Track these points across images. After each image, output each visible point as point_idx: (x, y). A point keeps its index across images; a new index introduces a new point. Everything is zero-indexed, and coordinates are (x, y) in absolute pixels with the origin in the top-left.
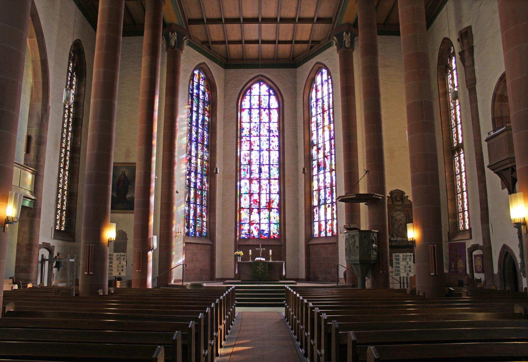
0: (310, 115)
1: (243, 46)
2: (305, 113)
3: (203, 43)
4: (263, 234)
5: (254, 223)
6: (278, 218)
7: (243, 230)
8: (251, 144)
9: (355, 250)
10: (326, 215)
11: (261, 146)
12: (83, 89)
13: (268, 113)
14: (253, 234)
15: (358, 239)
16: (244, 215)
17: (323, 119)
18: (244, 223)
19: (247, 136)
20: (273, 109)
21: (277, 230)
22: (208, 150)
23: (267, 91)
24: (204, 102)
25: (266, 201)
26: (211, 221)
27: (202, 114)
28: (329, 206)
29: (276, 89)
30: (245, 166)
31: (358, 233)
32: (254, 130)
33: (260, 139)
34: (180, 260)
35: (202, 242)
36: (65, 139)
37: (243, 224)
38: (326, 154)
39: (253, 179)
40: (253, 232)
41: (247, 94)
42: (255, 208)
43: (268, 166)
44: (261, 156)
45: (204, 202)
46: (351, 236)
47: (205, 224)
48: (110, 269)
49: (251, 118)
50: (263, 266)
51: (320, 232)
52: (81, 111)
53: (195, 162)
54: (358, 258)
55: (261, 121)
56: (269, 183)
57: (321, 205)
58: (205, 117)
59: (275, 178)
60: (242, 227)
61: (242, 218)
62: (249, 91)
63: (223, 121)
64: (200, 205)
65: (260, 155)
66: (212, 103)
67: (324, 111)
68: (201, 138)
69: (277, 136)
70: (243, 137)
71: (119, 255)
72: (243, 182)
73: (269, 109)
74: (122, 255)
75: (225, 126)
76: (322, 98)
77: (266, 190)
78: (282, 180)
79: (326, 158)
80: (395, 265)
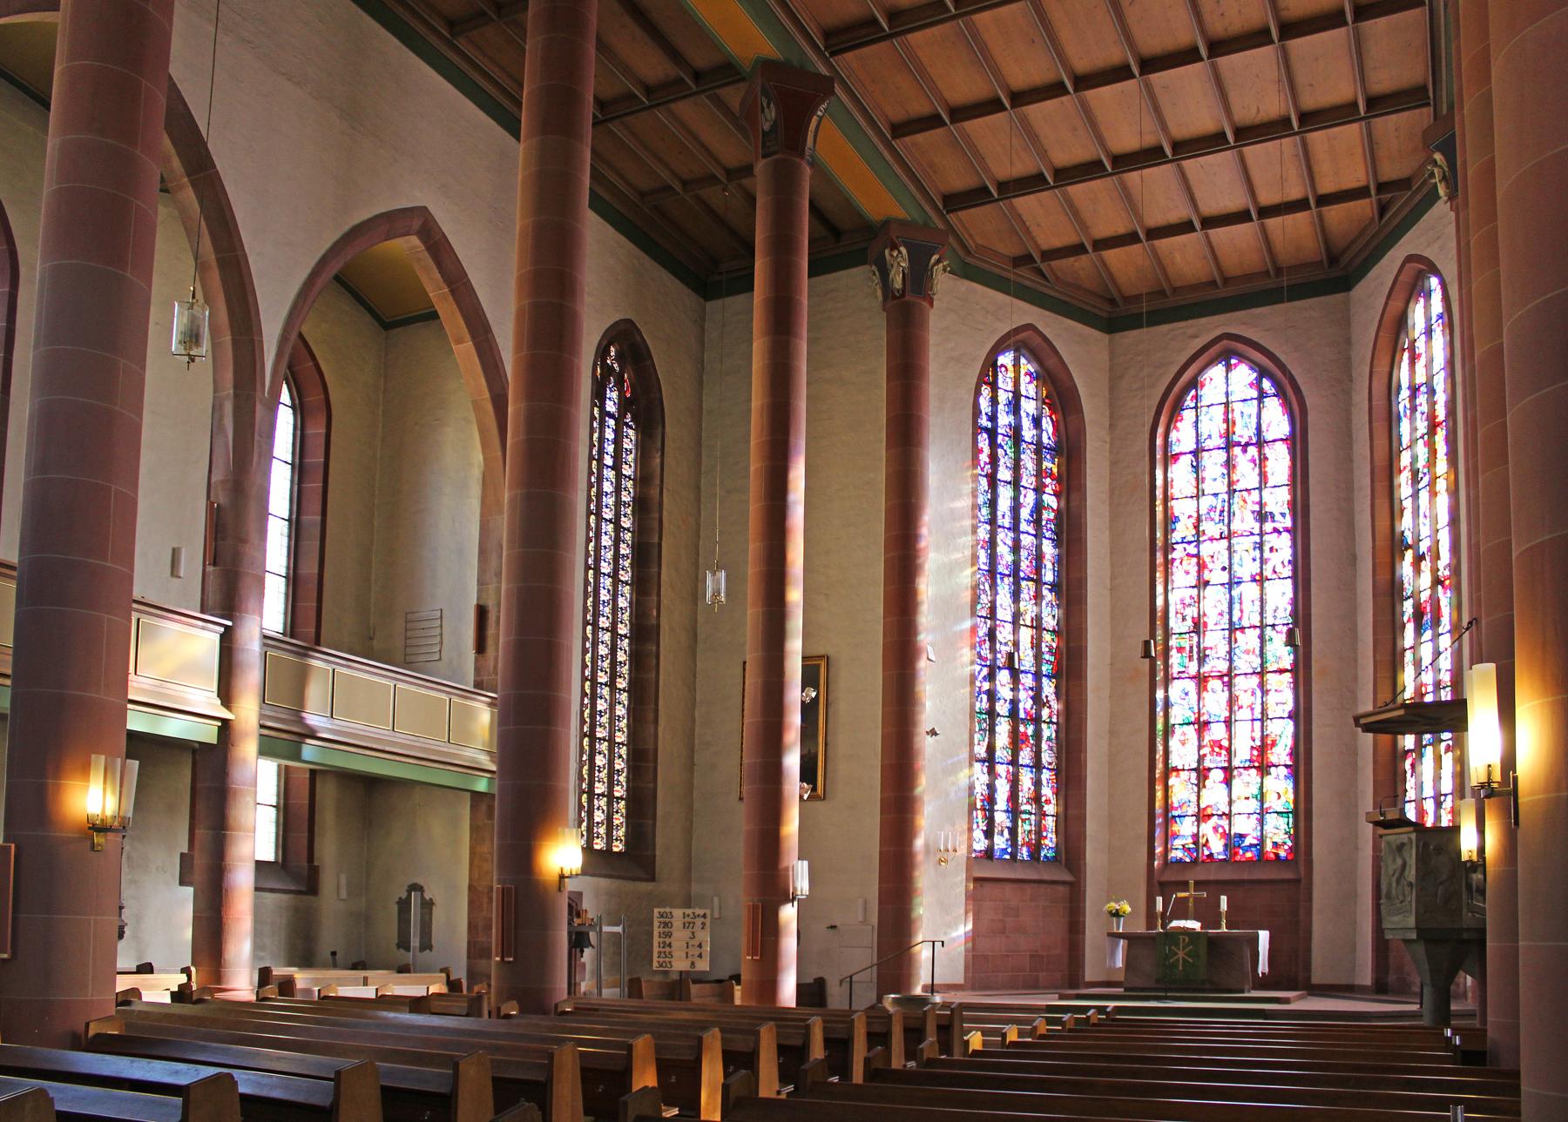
0: (1395, 445)
2: (1375, 442)
4: (1239, 846)
5: (1213, 815)
6: (1291, 797)
7: (1176, 836)
8: (1201, 566)
9: (1404, 896)
10: (1437, 779)
11: (1235, 567)
12: (658, 460)
13: (1257, 457)
14: (1209, 848)
16: (1181, 790)
17: (1433, 453)
18: (1179, 816)
19: (1189, 543)
20: (1274, 441)
21: (1286, 833)
22: (1058, 596)
23: (1251, 385)
24: (1039, 448)
25: (1253, 744)
26: (1071, 812)
27: (1034, 490)
28: (1448, 749)
29: (1278, 373)
30: (1183, 636)
31: (1413, 836)
32: (1212, 520)
34: (957, 930)
35: (1035, 877)
36: (610, 606)
37: (1177, 819)
38: (1440, 573)
40: (1207, 840)
41: (1186, 404)
42: (1217, 768)
43: (1258, 631)
44: (1236, 600)
45: (1047, 757)
46: (1394, 847)
47: (1050, 822)
48: (665, 952)
49: (1199, 480)
50: (1191, 947)
52: (656, 524)
54: (1411, 921)
55: (1235, 487)
56: (1262, 685)
57: (1426, 746)
58: (1045, 497)
59: (1281, 667)
60: (1175, 828)
61: (1175, 799)
62: (1193, 392)
63: (1107, 503)
65: (1231, 597)
66: (1069, 449)
67: (1433, 427)
68: (1031, 562)
69: (1286, 530)
70: (1175, 546)
71: (688, 915)
72: (1176, 689)
73: (1260, 443)
74: (699, 916)
75: (1115, 515)
77: (1252, 709)
79: (1440, 587)
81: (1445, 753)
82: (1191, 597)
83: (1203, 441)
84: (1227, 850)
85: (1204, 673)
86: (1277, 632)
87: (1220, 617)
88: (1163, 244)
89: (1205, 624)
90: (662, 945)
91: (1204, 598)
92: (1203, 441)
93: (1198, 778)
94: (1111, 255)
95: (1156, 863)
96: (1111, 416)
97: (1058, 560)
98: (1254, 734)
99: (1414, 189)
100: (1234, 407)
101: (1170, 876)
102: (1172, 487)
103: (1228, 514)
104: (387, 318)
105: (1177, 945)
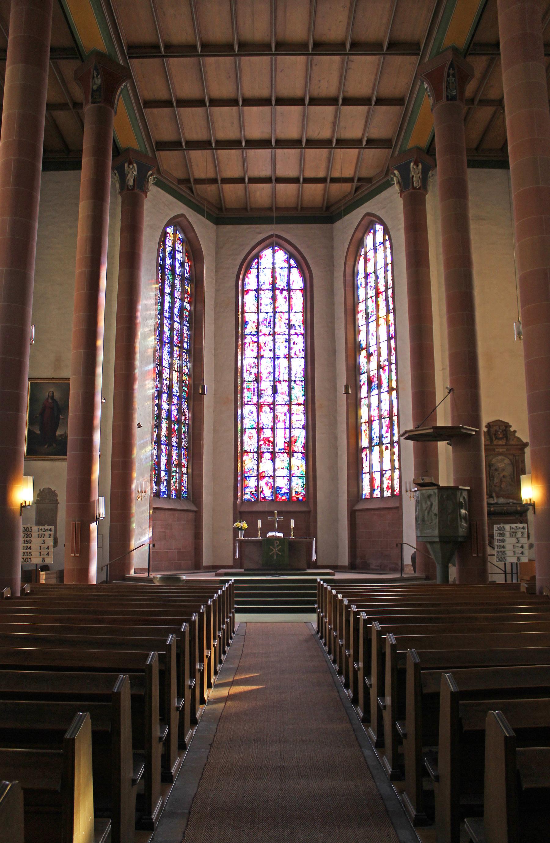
0: (356, 299)
1: (245, 186)
3: (181, 181)
4: (279, 494)
5: (265, 477)
6: (304, 468)
7: (247, 487)
8: (259, 348)
9: (432, 520)
10: (381, 462)
11: (276, 350)
13: (287, 296)
14: (264, 494)
15: (437, 501)
16: (249, 462)
17: (377, 306)
18: (248, 477)
19: (254, 335)
21: (302, 487)
22: (189, 356)
23: (285, 261)
24: (183, 279)
25: (285, 440)
28: (387, 448)
29: (299, 257)
30: (250, 383)
31: (436, 491)
32: (265, 325)
33: (274, 340)
34: (145, 537)
37: (247, 478)
38: (381, 363)
39: (263, 404)
40: (263, 490)
41: (253, 266)
43: (287, 383)
45: (184, 442)
47: (185, 477)
49: (259, 305)
50: (280, 547)
51: (372, 490)
53: (168, 376)
54: (436, 532)
55: (276, 310)
56: (290, 411)
57: (374, 446)
60: (246, 483)
61: (246, 468)
62: (256, 260)
64: (177, 447)
67: (378, 294)
69: (301, 334)
70: (246, 336)
71: (41, 530)
72: (247, 409)
73: (289, 290)
74: (47, 530)
76: (375, 272)
77: (285, 423)
78: (310, 406)
79: (381, 370)
80: (498, 544)
81: (385, 450)
82: (254, 363)
83: (261, 285)
84: (273, 495)
85: (261, 402)
86: (297, 384)
87: (268, 374)
88: (254, 186)
89: (261, 377)
90: (25, 548)
91: (261, 364)
92: (261, 285)
93: (258, 457)
94: (228, 188)
95: (238, 501)
96: (216, 267)
97: (190, 337)
98: (285, 435)
99: (373, 183)
100: (276, 271)
101: (244, 509)
102: (245, 307)
103: (273, 323)
104: (419, 186)
105: (273, 545)
